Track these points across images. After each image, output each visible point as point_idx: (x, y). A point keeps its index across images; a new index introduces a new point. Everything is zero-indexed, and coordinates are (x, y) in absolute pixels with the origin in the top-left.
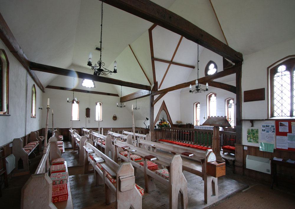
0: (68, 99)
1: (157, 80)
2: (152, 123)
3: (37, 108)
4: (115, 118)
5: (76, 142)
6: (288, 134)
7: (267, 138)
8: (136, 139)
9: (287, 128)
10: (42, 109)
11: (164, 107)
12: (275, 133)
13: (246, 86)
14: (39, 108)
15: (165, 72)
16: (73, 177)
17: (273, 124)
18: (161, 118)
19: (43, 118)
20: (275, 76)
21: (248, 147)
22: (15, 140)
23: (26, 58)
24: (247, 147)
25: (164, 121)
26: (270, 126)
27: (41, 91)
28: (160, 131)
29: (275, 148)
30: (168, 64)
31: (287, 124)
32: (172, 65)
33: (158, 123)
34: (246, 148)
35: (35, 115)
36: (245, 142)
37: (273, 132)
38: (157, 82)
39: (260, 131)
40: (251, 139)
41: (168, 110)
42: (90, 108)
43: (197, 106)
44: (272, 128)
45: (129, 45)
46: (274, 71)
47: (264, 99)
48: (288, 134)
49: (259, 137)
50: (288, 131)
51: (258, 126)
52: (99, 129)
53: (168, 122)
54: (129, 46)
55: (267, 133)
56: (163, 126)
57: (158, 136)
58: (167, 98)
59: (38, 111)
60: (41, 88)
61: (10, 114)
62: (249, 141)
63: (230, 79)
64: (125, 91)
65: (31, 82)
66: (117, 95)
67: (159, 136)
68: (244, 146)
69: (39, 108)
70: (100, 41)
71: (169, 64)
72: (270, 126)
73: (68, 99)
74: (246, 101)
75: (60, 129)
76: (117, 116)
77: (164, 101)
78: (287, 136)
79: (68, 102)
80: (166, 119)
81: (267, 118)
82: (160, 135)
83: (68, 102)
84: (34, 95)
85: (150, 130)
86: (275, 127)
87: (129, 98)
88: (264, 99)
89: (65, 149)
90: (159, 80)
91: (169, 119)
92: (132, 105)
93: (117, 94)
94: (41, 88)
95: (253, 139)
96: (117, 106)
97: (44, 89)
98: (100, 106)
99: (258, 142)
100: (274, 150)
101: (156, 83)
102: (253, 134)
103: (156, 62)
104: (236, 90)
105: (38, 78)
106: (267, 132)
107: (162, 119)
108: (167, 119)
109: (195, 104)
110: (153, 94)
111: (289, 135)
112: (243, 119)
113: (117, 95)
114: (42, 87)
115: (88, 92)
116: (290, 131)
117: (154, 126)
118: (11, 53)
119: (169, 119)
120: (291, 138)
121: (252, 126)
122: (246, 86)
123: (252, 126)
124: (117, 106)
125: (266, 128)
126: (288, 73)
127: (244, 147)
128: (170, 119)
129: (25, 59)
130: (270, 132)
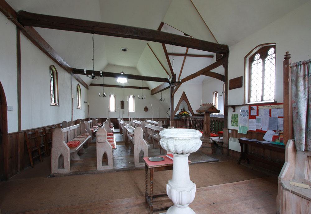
0: (99, 94)
1: (175, 73)
2: (173, 113)
3: (83, 102)
4: (146, 109)
5: (128, 135)
6: (256, 117)
7: (244, 122)
8: (131, 121)
9: (256, 112)
10: (86, 102)
11: (184, 97)
12: (248, 117)
13: (231, 77)
14: (84, 102)
15: (185, 63)
16: (170, 204)
17: (247, 108)
18: (181, 108)
19: (88, 109)
20: (253, 64)
21: (232, 130)
22: (63, 122)
23: (69, 66)
24: (230, 130)
25: (184, 110)
26: (246, 111)
27: (86, 88)
28: (181, 120)
29: (248, 130)
30: (183, 57)
31: (255, 108)
32: (187, 58)
33: (178, 112)
34: (230, 131)
35: (81, 107)
36: (230, 126)
37: (247, 116)
38: (175, 74)
39: (239, 116)
40: (234, 123)
41: (188, 100)
42: (124, 101)
43: (216, 96)
44: (247, 112)
45: (148, 44)
46: (252, 60)
47: (242, 87)
48: (256, 117)
49: (238, 121)
50: (256, 114)
51: (239, 111)
52: (129, 119)
53: (188, 112)
54: (147, 44)
55: (244, 117)
56: (183, 116)
57: (178, 125)
58: (183, 88)
59: (84, 104)
60: (85, 86)
61: (59, 105)
62: (233, 125)
63: (220, 70)
64: (153, 85)
65: (75, 83)
66: (148, 88)
67: (180, 125)
68: (229, 129)
69: (84, 102)
70: (92, 59)
71: (188, 53)
72: (246, 111)
73: (99, 94)
74: (230, 89)
75: (101, 118)
76: (148, 107)
77: (184, 92)
78: (255, 119)
79: (99, 96)
80: (186, 108)
81: (243, 104)
82: (180, 123)
83: (139, 98)
84: (79, 92)
85: (170, 119)
86: (248, 112)
87: (156, 90)
88: (242, 87)
89: (117, 142)
90: (176, 71)
91: (190, 109)
92: (159, 96)
93: (147, 87)
94: (85, 86)
95: (235, 124)
96: (99, 96)
97: (88, 86)
98: (133, 99)
99: (237, 126)
100: (248, 132)
101: (174, 76)
102: (235, 118)
103: (170, 57)
104: (223, 78)
105: (82, 78)
106: (244, 116)
107: (183, 109)
108: (188, 109)
109: (215, 93)
110: (172, 86)
111: (257, 118)
112: (229, 105)
113: (148, 88)
114: (86, 85)
115: (122, 87)
116: (258, 115)
117: (174, 116)
118: (59, 66)
119: (190, 109)
120: (258, 121)
121: (234, 111)
122: (231, 77)
123: (234, 111)
124: (139, 98)
125: (243, 113)
126: (261, 61)
127: (229, 130)
128: (190, 109)
129: (68, 67)
130: (245, 116)
